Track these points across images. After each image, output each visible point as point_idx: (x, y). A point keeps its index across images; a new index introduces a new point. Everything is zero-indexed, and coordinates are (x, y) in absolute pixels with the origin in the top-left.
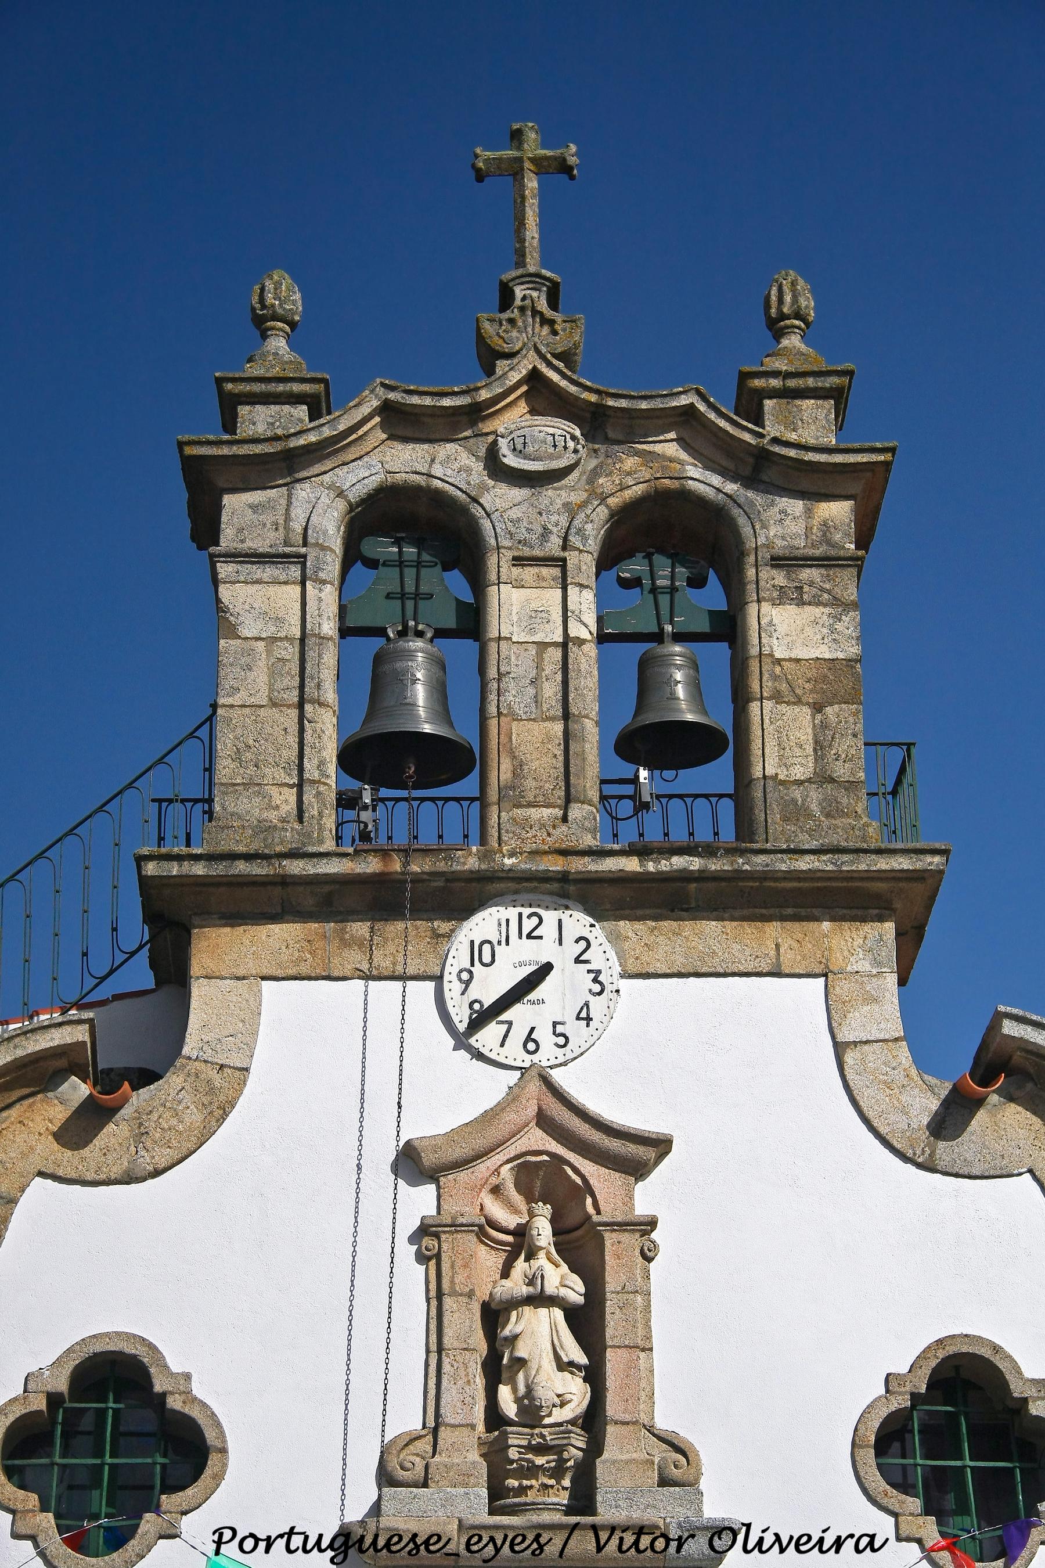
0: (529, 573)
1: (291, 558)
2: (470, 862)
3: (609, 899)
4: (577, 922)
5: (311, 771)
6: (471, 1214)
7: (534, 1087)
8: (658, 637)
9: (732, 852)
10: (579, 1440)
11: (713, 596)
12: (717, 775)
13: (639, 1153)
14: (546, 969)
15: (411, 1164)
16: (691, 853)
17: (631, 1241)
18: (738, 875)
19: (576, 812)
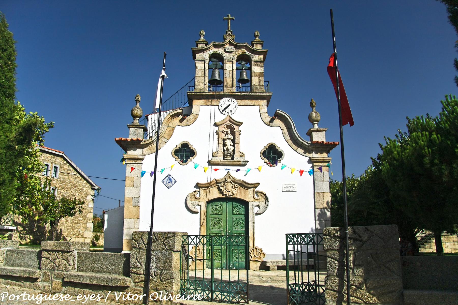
0: (229, 62)
1: (203, 60)
2: (222, 93)
3: (237, 97)
4: (233, 100)
5: (205, 83)
6: (222, 130)
7: (228, 117)
8: (242, 70)
9: (250, 93)
10: (232, 153)
11: (248, 65)
12: (248, 84)
13: (239, 124)
14: (230, 105)
15: (215, 125)
16: (245, 92)
17: (238, 133)
18: (250, 95)
19: (233, 88)
